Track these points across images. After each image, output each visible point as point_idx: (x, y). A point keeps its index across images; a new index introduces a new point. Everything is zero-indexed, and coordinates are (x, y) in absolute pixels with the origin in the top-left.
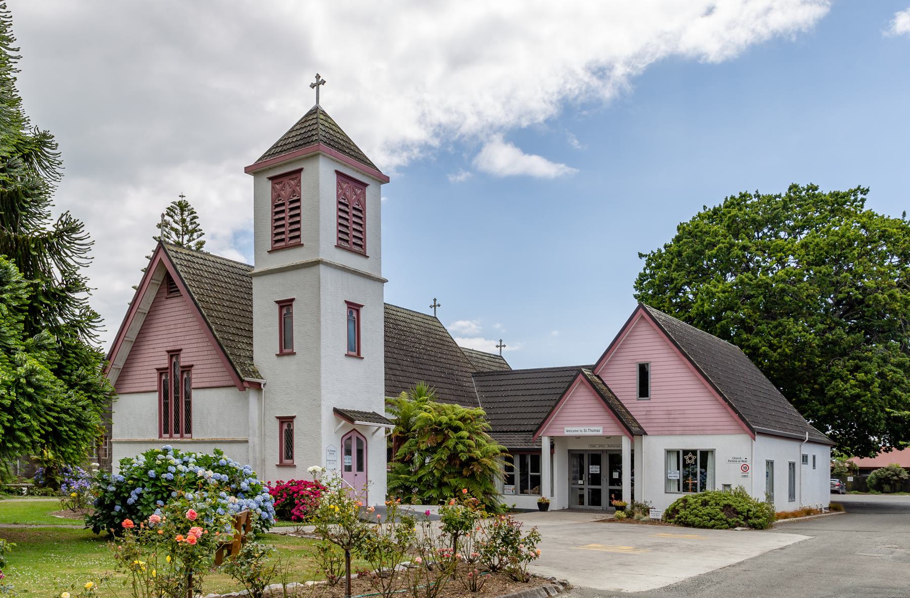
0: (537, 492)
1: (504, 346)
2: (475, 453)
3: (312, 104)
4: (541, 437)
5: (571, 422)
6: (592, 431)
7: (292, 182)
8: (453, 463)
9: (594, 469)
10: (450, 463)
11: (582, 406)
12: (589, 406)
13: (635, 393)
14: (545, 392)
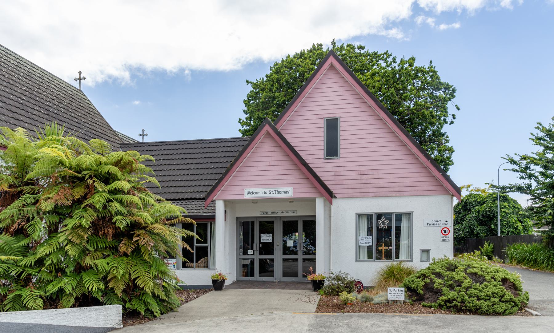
0: (202, 265)
1: (147, 135)
2: (141, 216)
4: (215, 201)
5: (252, 183)
6: (280, 193)
8: (101, 233)
9: (266, 238)
10: (96, 233)
11: (267, 164)
12: (276, 163)
13: (322, 152)
14: (202, 161)
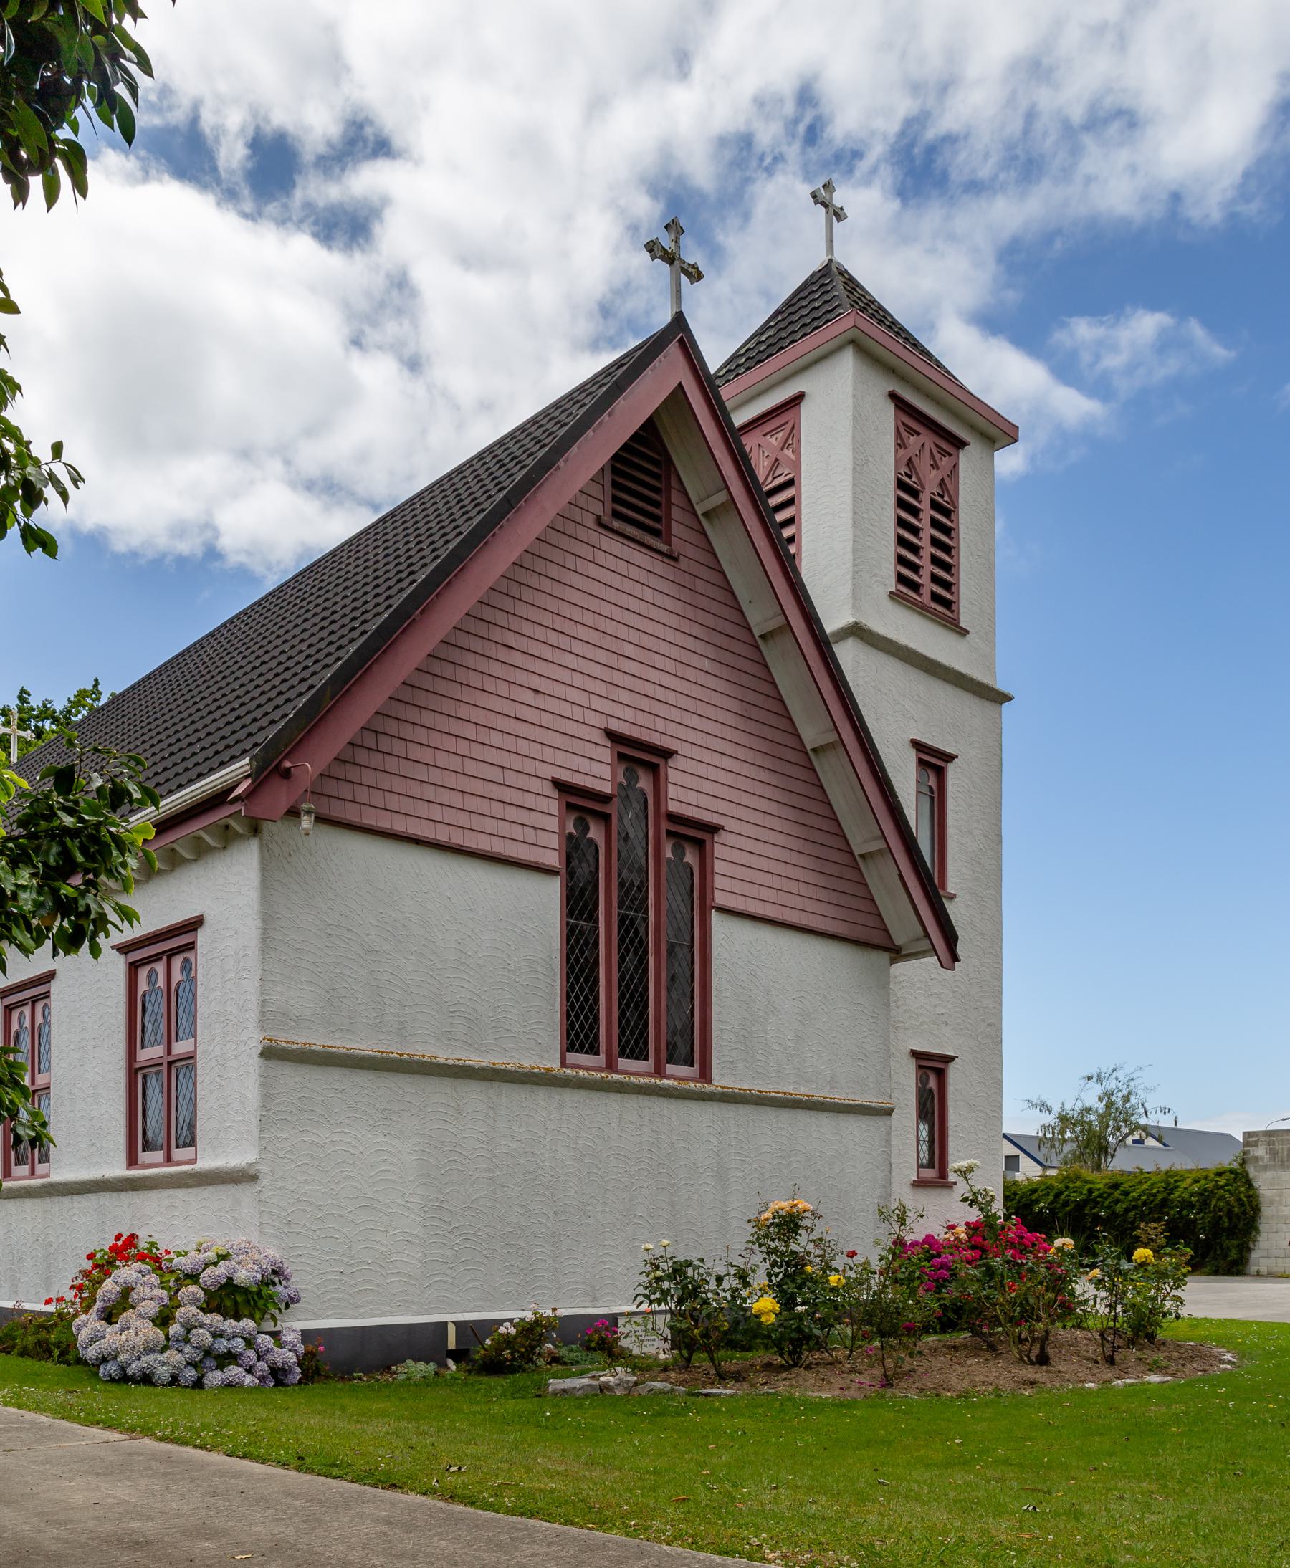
3: (817, 261)
7: (773, 440)
